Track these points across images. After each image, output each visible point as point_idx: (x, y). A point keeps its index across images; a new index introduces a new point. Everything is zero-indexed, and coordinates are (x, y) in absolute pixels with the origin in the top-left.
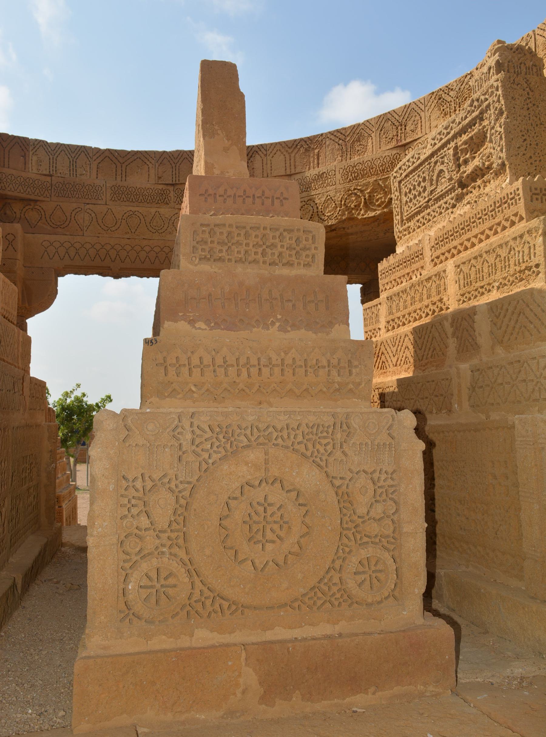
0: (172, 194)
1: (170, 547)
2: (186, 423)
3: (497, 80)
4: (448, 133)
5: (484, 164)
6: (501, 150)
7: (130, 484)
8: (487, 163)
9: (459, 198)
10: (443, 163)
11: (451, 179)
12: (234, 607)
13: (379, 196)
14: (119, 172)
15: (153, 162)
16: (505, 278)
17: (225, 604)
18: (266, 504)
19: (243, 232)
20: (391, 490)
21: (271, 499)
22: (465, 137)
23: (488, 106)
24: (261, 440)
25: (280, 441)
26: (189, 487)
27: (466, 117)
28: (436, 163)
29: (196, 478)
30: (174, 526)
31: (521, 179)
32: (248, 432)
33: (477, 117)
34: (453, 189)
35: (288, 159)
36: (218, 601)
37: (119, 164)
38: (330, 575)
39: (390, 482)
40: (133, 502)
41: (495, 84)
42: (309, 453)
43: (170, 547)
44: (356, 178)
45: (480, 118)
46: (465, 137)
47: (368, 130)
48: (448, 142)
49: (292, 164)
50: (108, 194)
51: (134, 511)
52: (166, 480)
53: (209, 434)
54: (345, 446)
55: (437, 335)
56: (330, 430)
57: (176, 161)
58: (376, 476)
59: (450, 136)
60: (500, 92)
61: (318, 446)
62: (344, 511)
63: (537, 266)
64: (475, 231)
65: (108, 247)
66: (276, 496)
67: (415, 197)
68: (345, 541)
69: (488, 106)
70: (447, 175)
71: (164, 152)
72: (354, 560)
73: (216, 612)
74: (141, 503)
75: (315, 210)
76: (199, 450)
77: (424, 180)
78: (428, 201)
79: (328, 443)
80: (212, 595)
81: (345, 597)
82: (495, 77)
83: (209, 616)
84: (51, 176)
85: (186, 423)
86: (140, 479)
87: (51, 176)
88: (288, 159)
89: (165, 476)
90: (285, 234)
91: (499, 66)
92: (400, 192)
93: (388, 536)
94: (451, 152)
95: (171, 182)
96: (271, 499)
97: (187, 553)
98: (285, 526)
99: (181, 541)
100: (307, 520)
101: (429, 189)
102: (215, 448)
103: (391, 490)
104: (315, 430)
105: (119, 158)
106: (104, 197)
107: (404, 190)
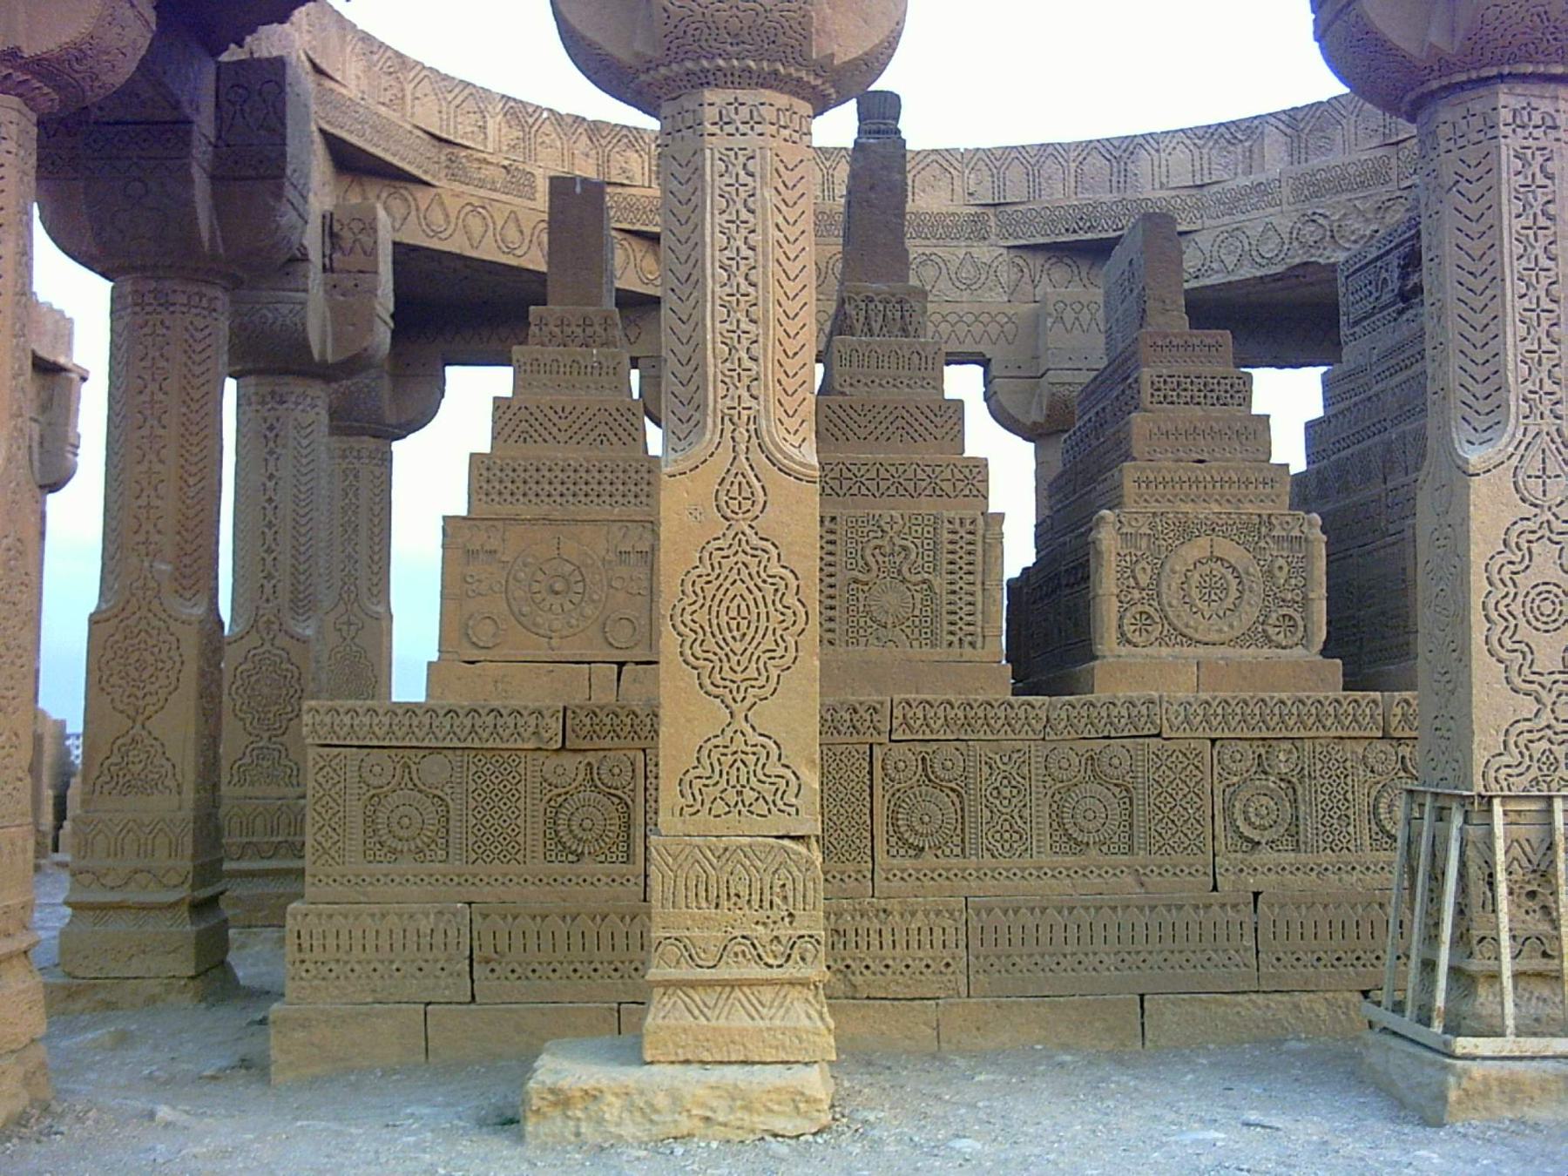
9: (1401, 312)
18: (1211, 574)
34: (1394, 303)
35: (1197, 157)
44: (1315, 195)
49: (1206, 166)
72: (1274, 615)
75: (1247, 247)
88: (1197, 157)
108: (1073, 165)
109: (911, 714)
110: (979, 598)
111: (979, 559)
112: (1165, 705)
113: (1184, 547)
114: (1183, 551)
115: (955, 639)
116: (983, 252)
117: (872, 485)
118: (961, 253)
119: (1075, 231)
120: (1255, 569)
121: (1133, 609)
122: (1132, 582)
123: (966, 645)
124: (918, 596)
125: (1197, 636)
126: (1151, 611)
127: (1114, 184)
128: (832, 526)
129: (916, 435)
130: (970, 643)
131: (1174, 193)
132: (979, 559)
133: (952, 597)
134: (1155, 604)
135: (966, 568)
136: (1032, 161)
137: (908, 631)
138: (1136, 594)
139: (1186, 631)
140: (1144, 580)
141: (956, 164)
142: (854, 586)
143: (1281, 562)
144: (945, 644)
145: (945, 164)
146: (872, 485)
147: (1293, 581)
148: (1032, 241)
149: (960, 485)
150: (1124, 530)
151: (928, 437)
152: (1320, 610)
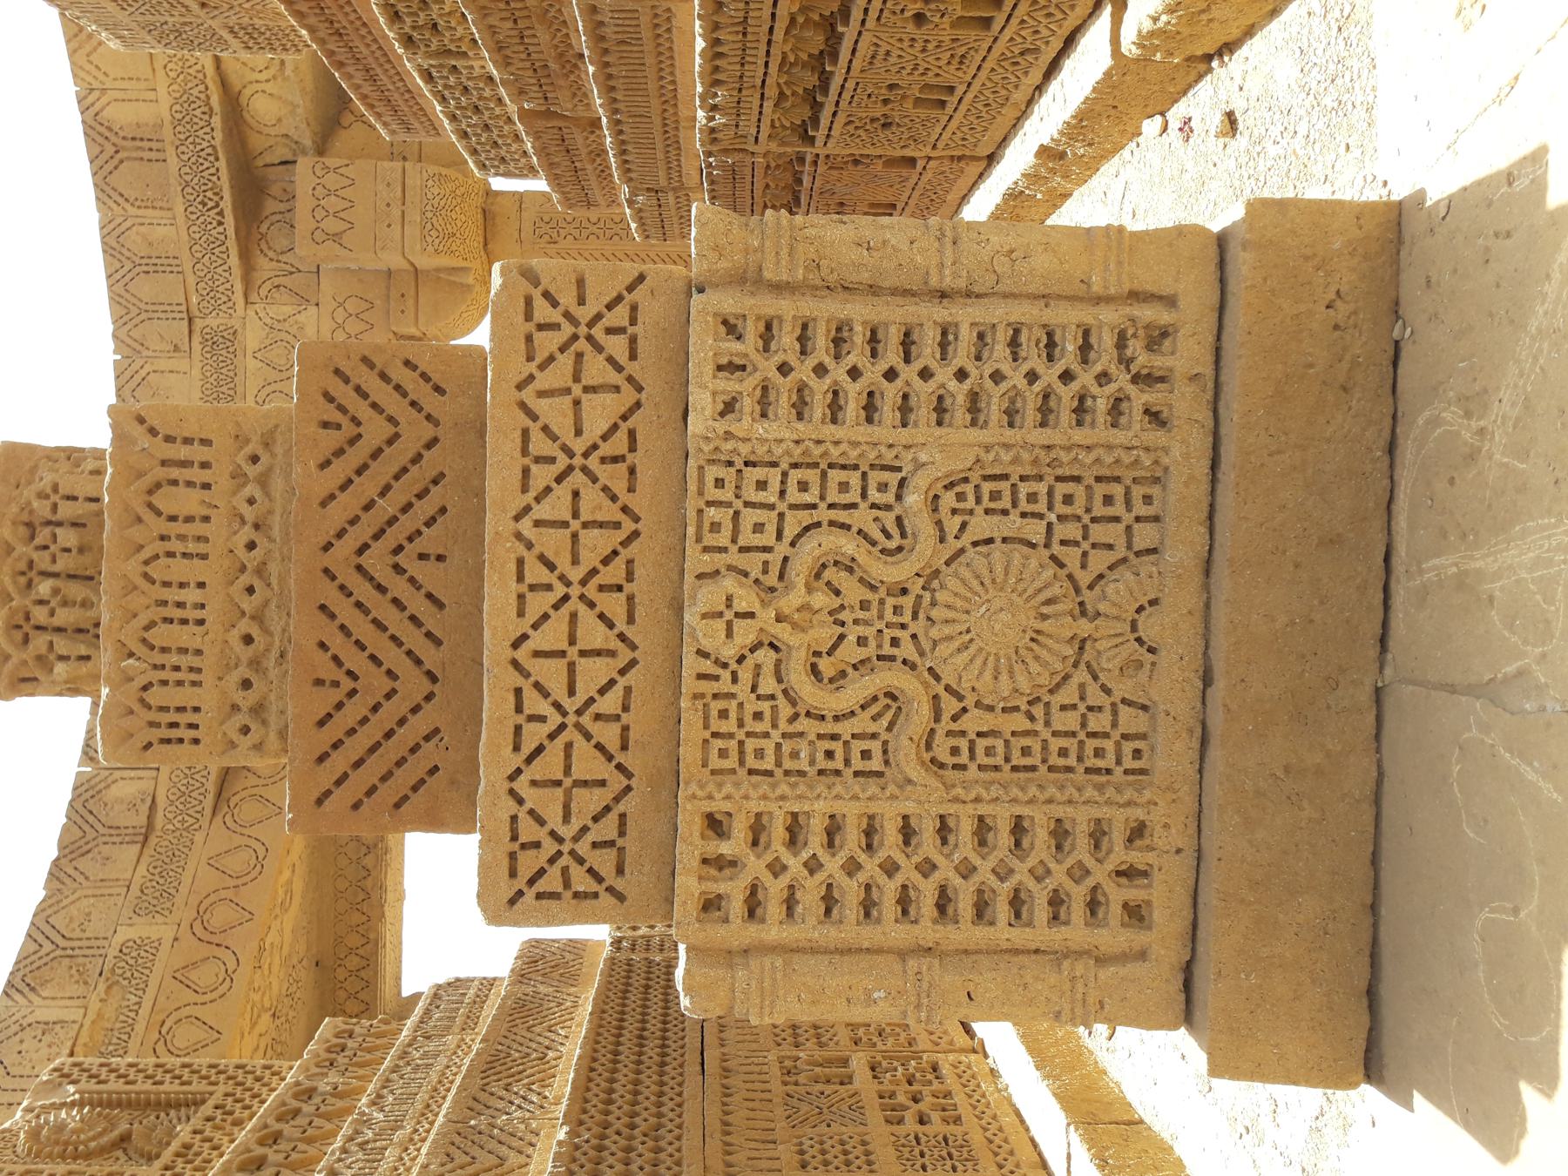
0: (213, 321)
57: (135, 311)
95: (186, 322)
108: (132, 211)
110: (998, 313)
111: (859, 312)
115: (1140, 398)
116: (253, 337)
118: (252, 364)
119: (221, 213)
123: (1159, 362)
124: (981, 525)
127: (153, 155)
128: (740, 829)
129: (425, 508)
130: (1153, 345)
131: (160, 73)
132: (859, 312)
133: (994, 409)
136: (129, 265)
137: (1099, 560)
141: (135, 366)
142: (942, 751)
144: (1156, 437)
145: (138, 378)
146: (593, 673)
148: (237, 272)
149: (596, 369)
151: (427, 469)
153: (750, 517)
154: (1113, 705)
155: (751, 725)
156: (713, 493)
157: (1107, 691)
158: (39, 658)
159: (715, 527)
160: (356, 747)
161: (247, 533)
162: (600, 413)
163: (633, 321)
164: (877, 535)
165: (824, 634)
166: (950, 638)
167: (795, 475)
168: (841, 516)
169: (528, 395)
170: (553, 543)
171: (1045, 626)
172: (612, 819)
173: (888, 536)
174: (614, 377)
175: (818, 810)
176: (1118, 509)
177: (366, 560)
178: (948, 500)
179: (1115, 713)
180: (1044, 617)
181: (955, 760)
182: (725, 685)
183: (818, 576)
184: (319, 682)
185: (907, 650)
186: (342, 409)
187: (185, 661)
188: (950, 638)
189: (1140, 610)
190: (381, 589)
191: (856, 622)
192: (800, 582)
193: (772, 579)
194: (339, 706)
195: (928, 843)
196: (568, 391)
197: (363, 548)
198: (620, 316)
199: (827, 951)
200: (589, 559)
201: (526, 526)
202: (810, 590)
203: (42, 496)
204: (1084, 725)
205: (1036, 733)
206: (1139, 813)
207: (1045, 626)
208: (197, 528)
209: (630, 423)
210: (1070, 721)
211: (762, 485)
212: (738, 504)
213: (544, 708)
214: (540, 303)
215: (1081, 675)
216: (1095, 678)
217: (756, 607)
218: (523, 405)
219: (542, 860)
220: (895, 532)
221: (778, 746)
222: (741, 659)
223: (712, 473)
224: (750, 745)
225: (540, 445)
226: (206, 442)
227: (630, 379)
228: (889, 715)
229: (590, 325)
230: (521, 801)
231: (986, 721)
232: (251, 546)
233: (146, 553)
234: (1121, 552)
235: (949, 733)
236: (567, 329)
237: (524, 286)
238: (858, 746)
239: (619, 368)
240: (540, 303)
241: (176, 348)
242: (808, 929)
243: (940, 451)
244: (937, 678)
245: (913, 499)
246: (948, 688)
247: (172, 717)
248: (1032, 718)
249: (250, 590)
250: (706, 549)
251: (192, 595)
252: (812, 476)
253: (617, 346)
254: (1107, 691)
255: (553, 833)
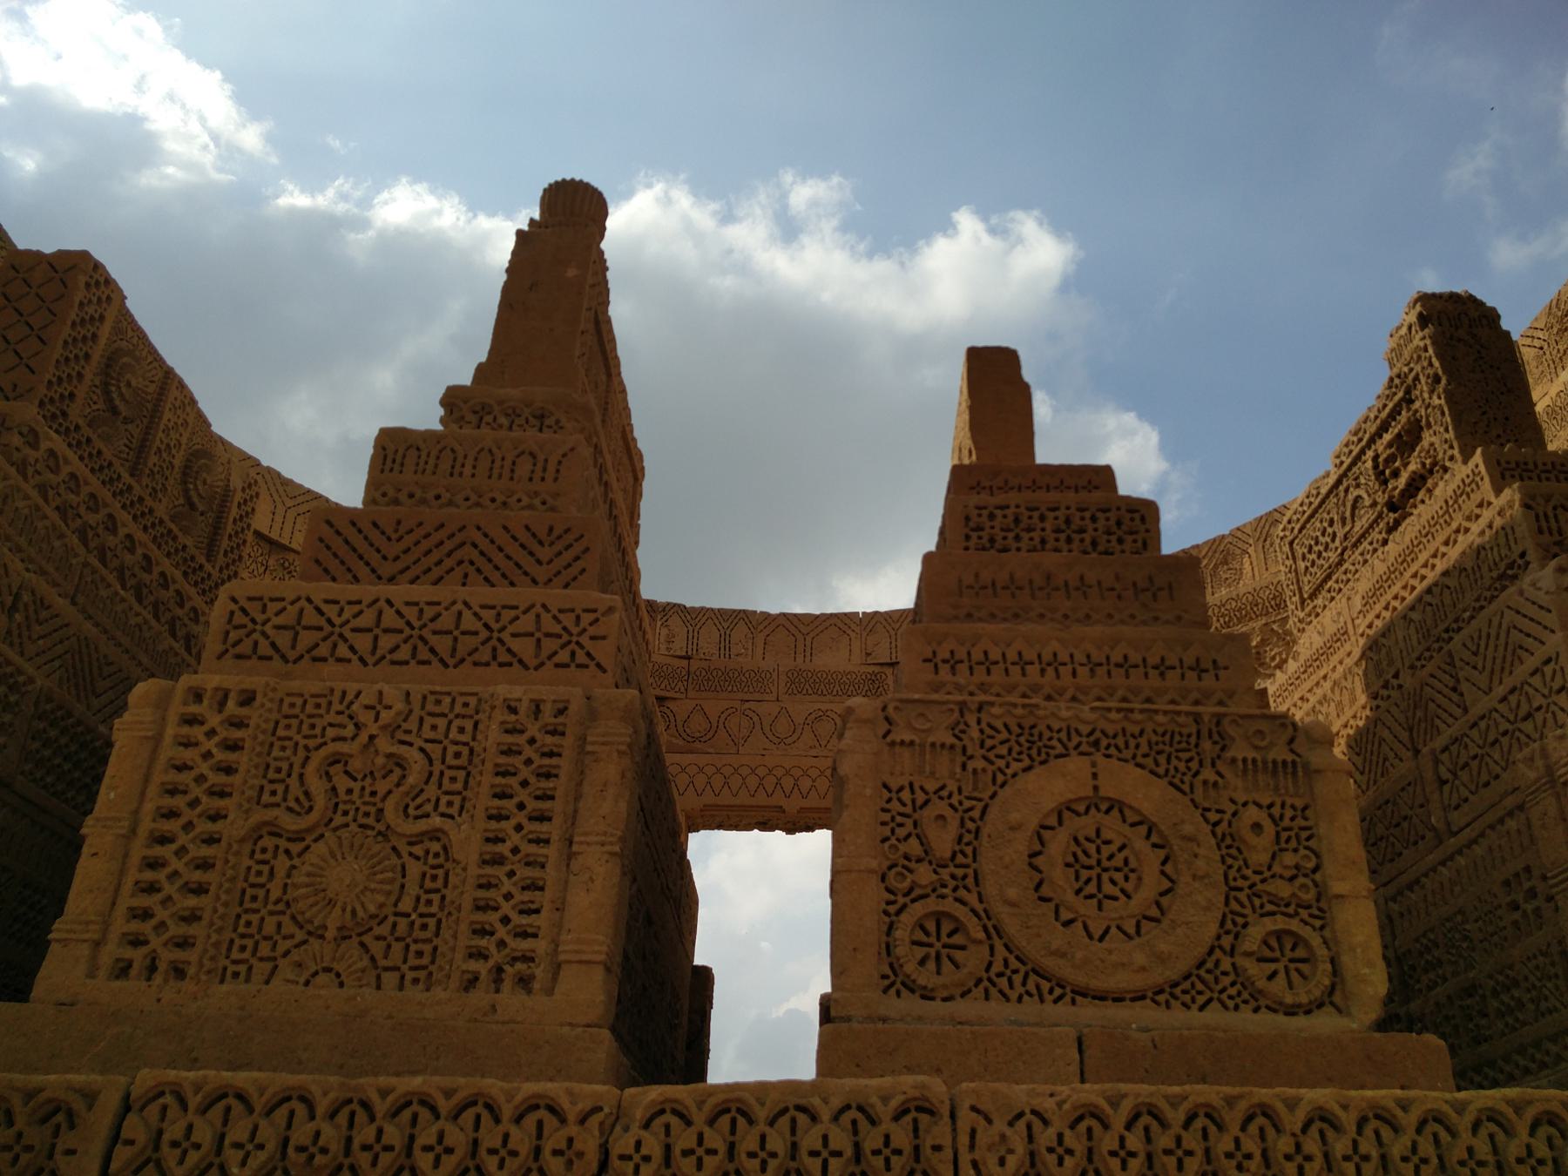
0: (890, 680)
1: (955, 889)
2: (971, 719)
3: (1423, 338)
4: (1360, 440)
5: (1424, 465)
6: (1447, 430)
7: (894, 795)
8: (1428, 462)
10: (1358, 486)
11: (1374, 504)
12: (1058, 991)
13: (1276, 650)
14: (800, 648)
15: (857, 629)
16: (1478, 600)
17: (1045, 986)
19: (1036, 514)
20: (1304, 834)
21: (1106, 835)
22: (1387, 437)
23: (1416, 378)
24: (1084, 748)
25: (1112, 751)
26: (980, 805)
27: (1385, 406)
28: (1347, 491)
29: (990, 793)
30: (960, 859)
31: (1479, 450)
32: (1063, 735)
33: (1402, 399)
36: (1033, 978)
37: (799, 636)
38: (1214, 958)
39: (1300, 822)
40: (899, 819)
41: (1422, 344)
42: (1161, 771)
43: (955, 889)
45: (1408, 400)
46: (1387, 437)
47: (1240, 544)
48: (1362, 452)
50: (782, 684)
51: (901, 832)
52: (944, 793)
53: (1005, 735)
54: (1218, 763)
55: (1386, 734)
56: (1193, 740)
58: (1276, 811)
59: (1364, 443)
60: (1431, 351)
61: (1174, 762)
62: (1229, 861)
63: (1523, 555)
64: (1423, 557)
65: (779, 772)
66: (1113, 828)
67: (1319, 555)
68: (1235, 906)
69: (1416, 378)
70: (1367, 502)
71: (876, 613)
73: (1029, 994)
74: (909, 822)
76: (991, 755)
77: (1331, 523)
78: (1342, 554)
79: (1191, 759)
80: (1023, 969)
81: (1245, 995)
82: (1421, 334)
83: (1020, 999)
84: (689, 658)
85: (971, 719)
86: (907, 790)
87: (689, 658)
89: (943, 788)
90: (1099, 515)
91: (1423, 320)
92: (1294, 558)
93: (1308, 907)
94: (1369, 464)
96: (1106, 835)
97: (981, 901)
98: (1132, 875)
99: (970, 881)
100: (1168, 868)
101: (1340, 535)
102: (1014, 755)
103: (1304, 834)
104: (1167, 737)
105: (801, 627)
106: (774, 689)
107: (1299, 551)
109: (174, 1131)
110: (551, 875)
112: (966, 1119)
113: (1031, 775)
114: (1030, 781)
117: (363, 643)
120: (1193, 824)
121: (918, 909)
122: (914, 847)
124: (414, 869)
125: (1080, 978)
126: (960, 912)
134: (972, 899)
135: (532, 805)
137: (377, 948)
138: (924, 875)
139: (1050, 963)
140: (943, 841)
142: (268, 842)
143: (1252, 814)
145: (845, 628)
147: (1289, 859)
149: (549, 645)
150: (896, 736)
152: (1359, 926)
153: (442, 723)
154: (275, 959)
155: (307, 722)
156: (460, 700)
157: (286, 954)
158: (463, 418)
159: (438, 702)
160: (357, 541)
161: (500, 498)
162: (524, 648)
163: (578, 666)
164: (419, 801)
165: (356, 765)
166: (341, 845)
167: (465, 751)
168: (434, 779)
169: (538, 609)
170: (446, 621)
171: (338, 909)
172: (270, 652)
173: (417, 808)
174: (544, 654)
175: (243, 760)
176: (412, 961)
177: (468, 548)
178: (435, 847)
179: (269, 959)
180: (344, 910)
181: (258, 849)
182: (336, 707)
183: (398, 764)
184: (399, 523)
185: (339, 820)
186: (559, 537)
187: (430, 467)
188: (341, 845)
189: (338, 975)
190: (449, 555)
191: (363, 788)
192: (394, 749)
193: (400, 735)
194: (383, 533)
195: (204, 827)
196: (538, 629)
197: (475, 546)
198: (581, 657)
199: (149, 767)
200: (433, 640)
201: (459, 606)
202: (389, 756)
203: (558, 422)
204: (265, 938)
205: (266, 904)
206: (191, 971)
207: (338, 909)
208: (506, 473)
209: (516, 664)
210: (269, 928)
211: (462, 730)
212: (451, 716)
213: (346, 616)
214: (592, 616)
215: (300, 936)
216: (297, 946)
217: (380, 723)
218: (533, 606)
219: (253, 614)
220: (419, 812)
221: (290, 739)
222: (351, 717)
223: (473, 701)
224: (295, 722)
225: (507, 615)
226: (556, 480)
227: (542, 664)
228: (297, 808)
229: (578, 643)
230: (292, 603)
231: (280, 873)
232: (493, 500)
233: (495, 450)
234: (382, 963)
235: (277, 847)
236: (575, 630)
237: (602, 609)
238: (280, 788)
239: (549, 658)
240: (592, 616)
241: (868, 654)
242: (168, 751)
243: (466, 837)
244: (316, 840)
245: (437, 821)
246: (308, 847)
247: (399, 460)
248: (277, 902)
249: (467, 499)
250: (425, 698)
251: (468, 471)
252: (463, 761)
253: (563, 656)
254: (286, 954)
255: (269, 620)
